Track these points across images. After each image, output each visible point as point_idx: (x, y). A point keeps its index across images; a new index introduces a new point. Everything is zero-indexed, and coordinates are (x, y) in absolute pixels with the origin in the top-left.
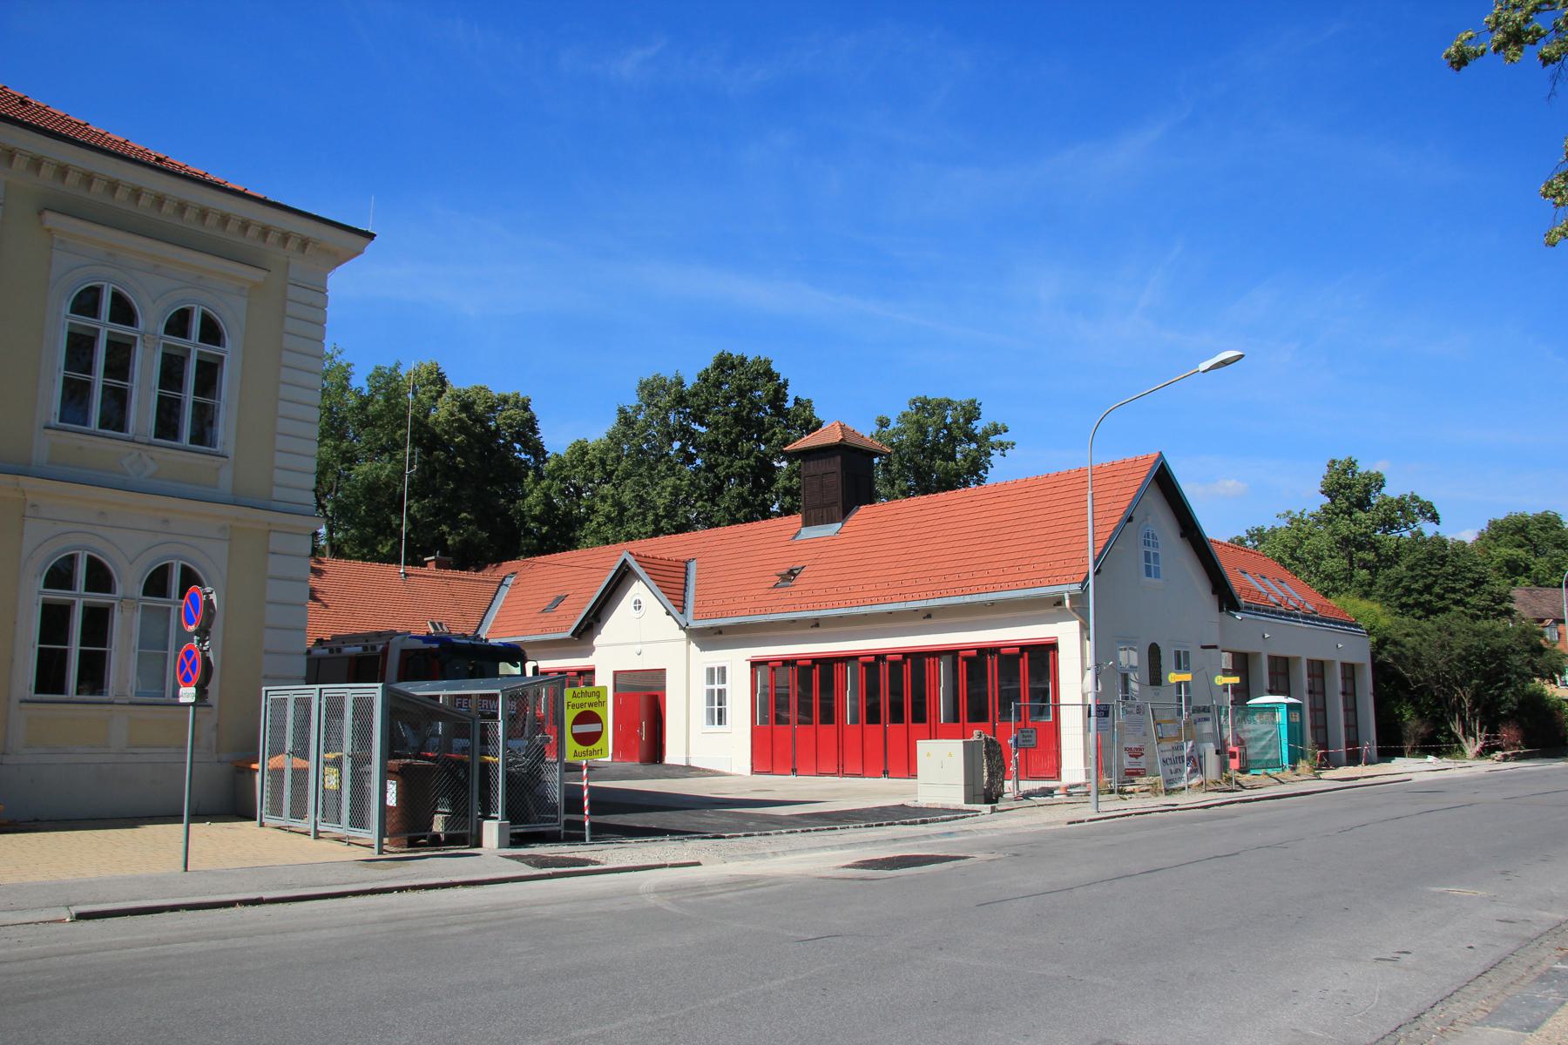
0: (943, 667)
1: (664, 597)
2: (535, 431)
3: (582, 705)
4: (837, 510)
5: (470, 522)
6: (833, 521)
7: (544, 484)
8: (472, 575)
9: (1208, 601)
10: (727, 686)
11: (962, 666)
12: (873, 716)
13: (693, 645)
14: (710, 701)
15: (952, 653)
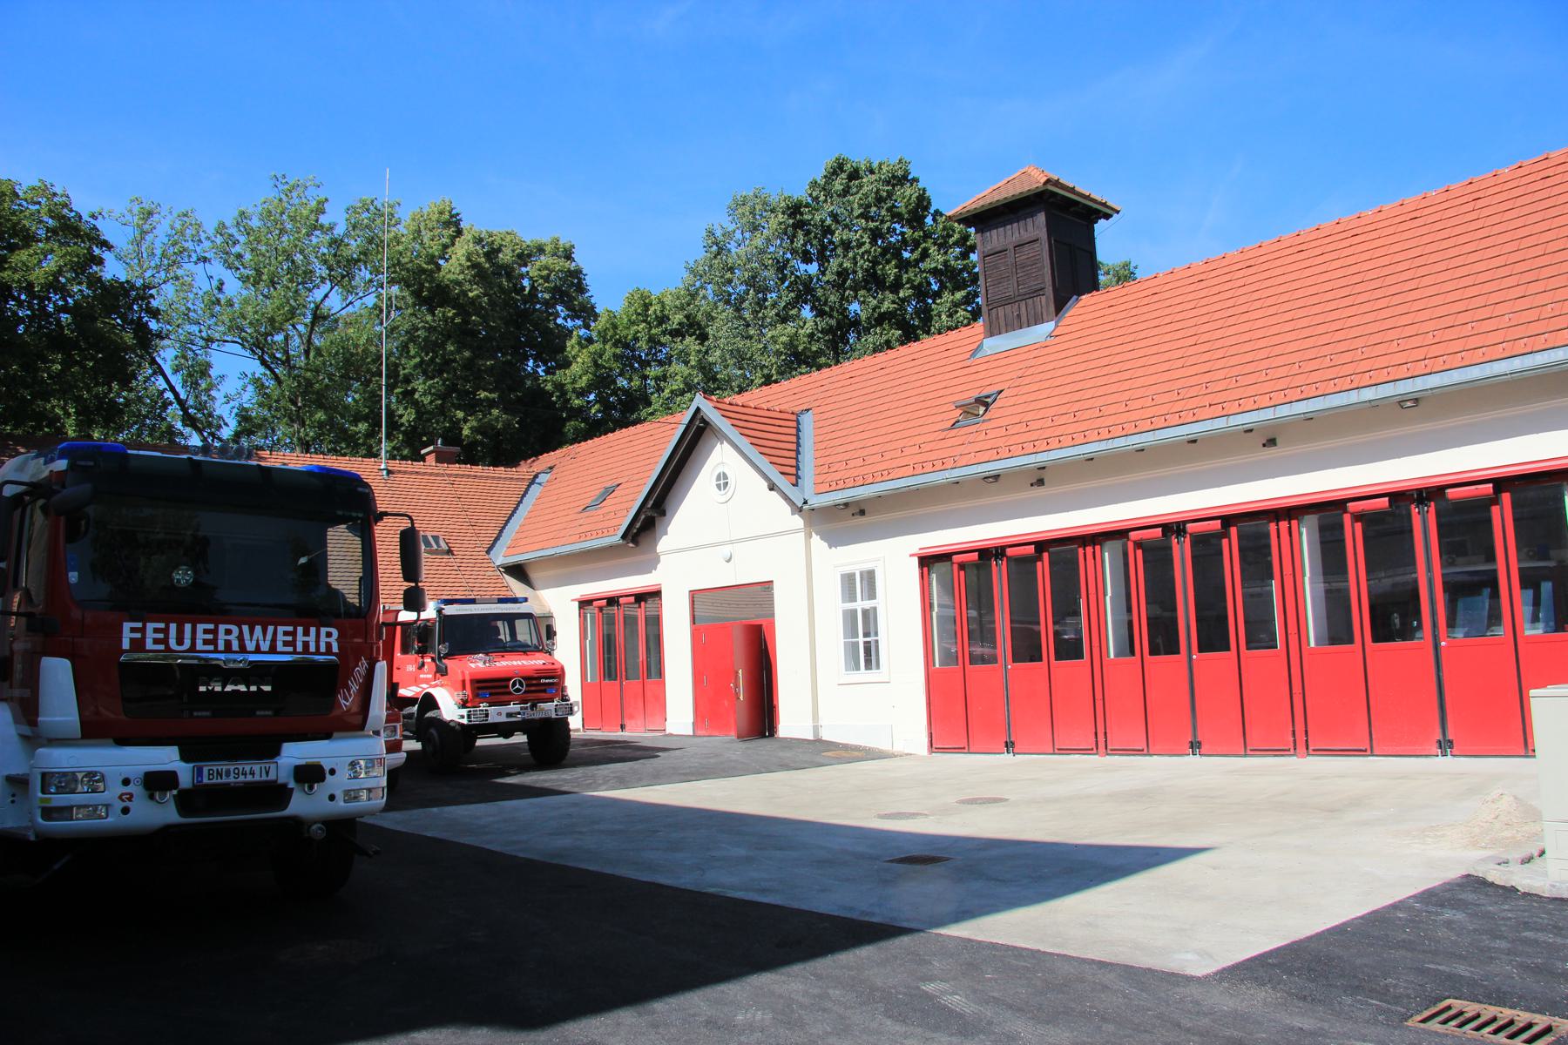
0: (1306, 535)
1: (763, 462)
2: (581, 289)
4: (1046, 301)
5: (492, 404)
6: (1038, 320)
7: (596, 347)
8: (501, 471)
11: (1353, 535)
12: (1164, 639)
13: (816, 539)
14: (851, 630)
15: (1328, 510)
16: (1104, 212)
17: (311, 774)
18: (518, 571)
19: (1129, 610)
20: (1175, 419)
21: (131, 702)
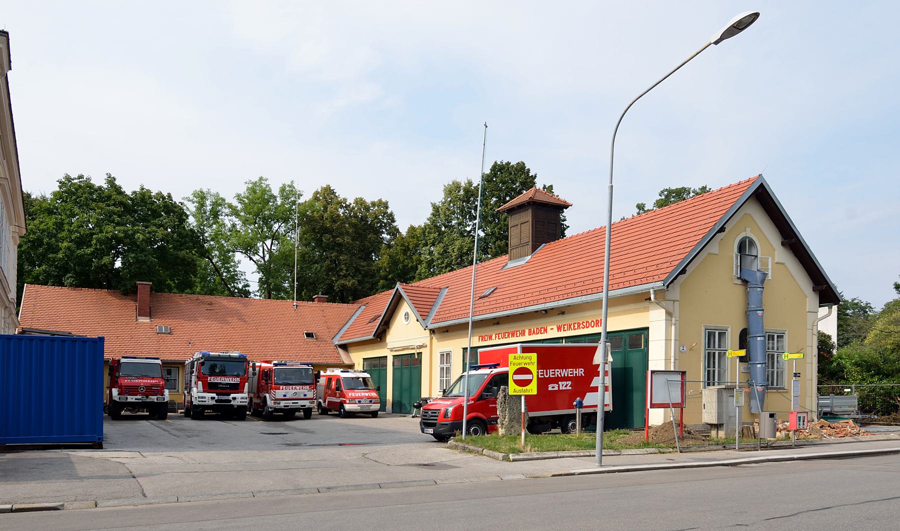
16: (567, 206)
17: (234, 398)
18: (344, 347)
19: (709, 367)
20: (532, 303)
21: (209, 388)
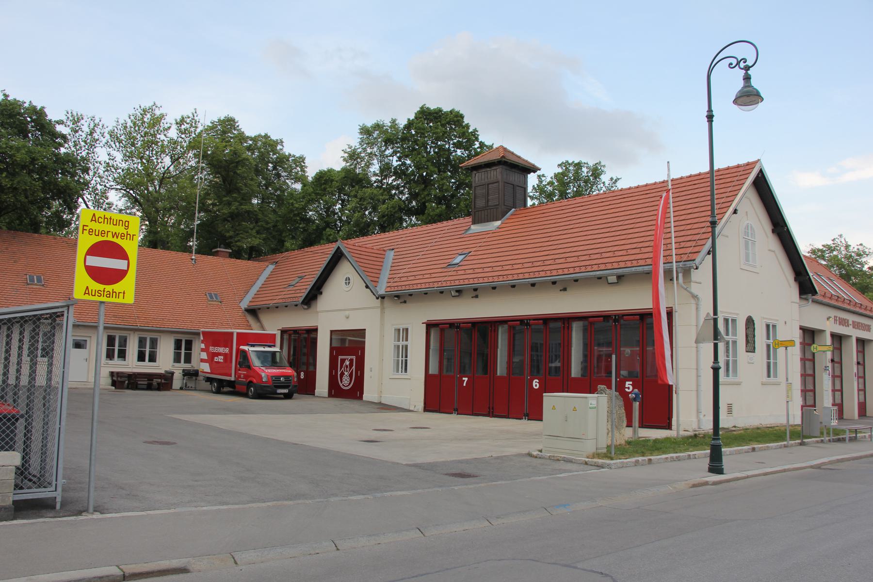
3: (103, 233)
9: (793, 290)
10: (409, 343)
19: (768, 357)
